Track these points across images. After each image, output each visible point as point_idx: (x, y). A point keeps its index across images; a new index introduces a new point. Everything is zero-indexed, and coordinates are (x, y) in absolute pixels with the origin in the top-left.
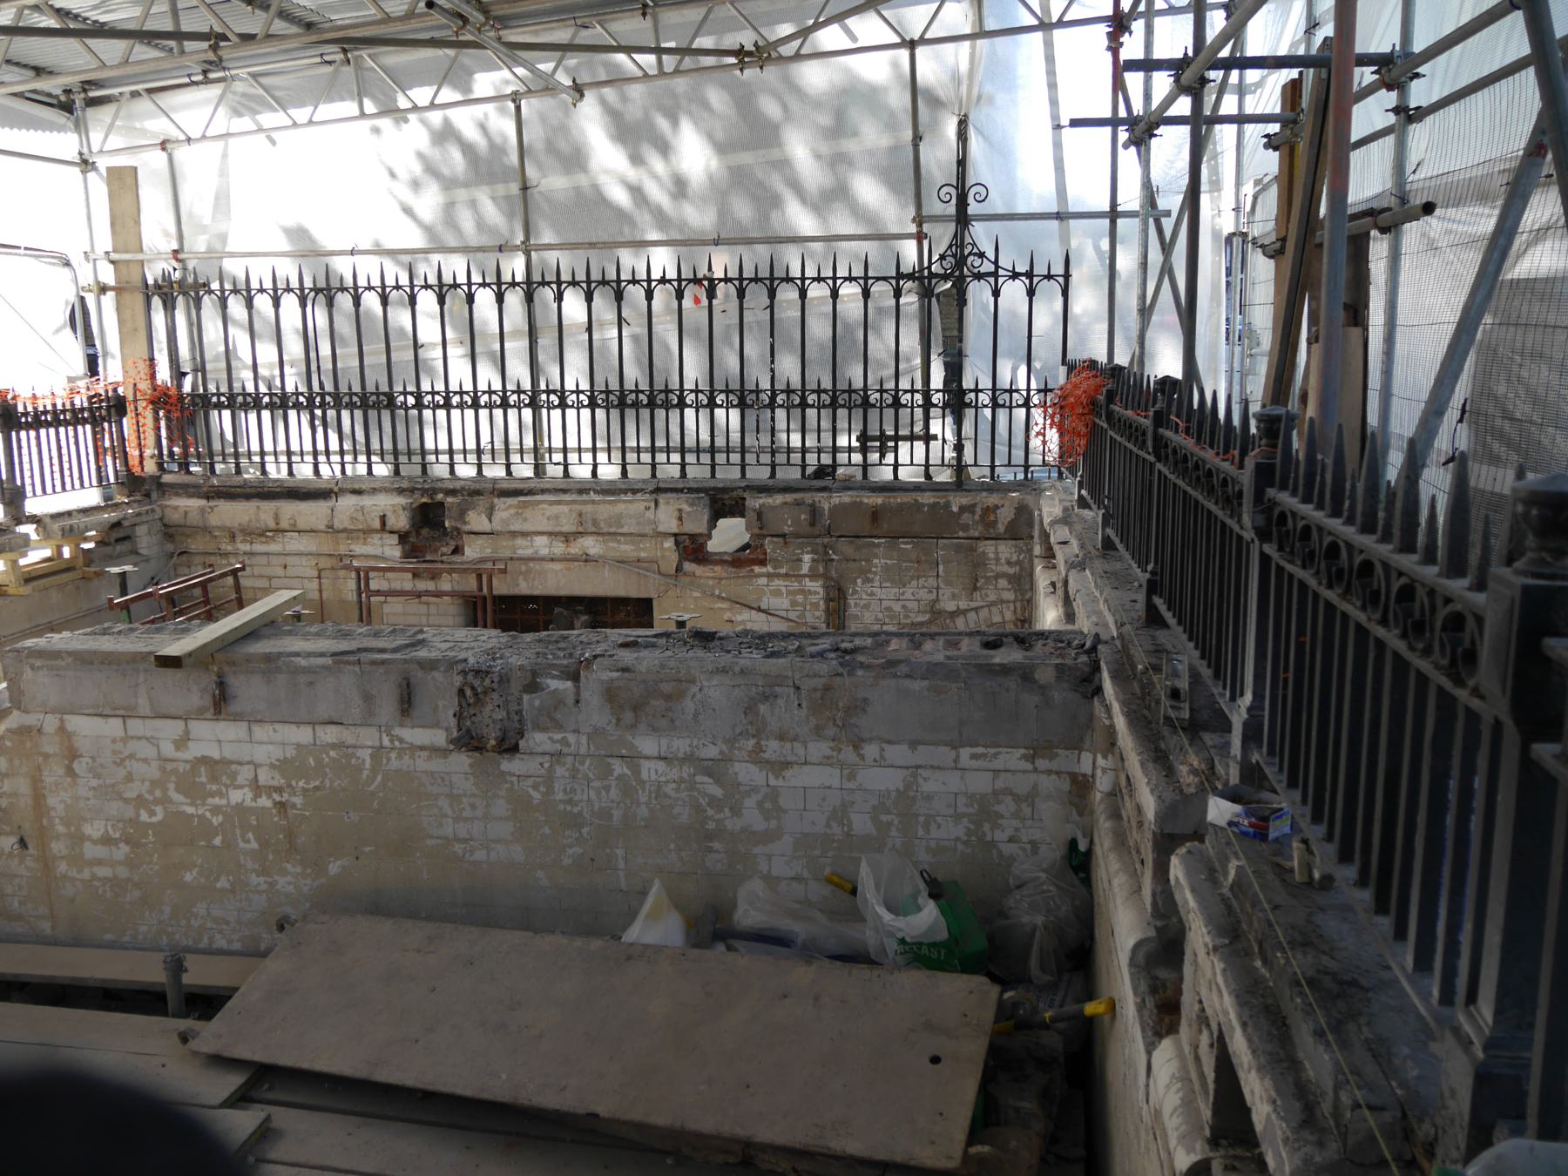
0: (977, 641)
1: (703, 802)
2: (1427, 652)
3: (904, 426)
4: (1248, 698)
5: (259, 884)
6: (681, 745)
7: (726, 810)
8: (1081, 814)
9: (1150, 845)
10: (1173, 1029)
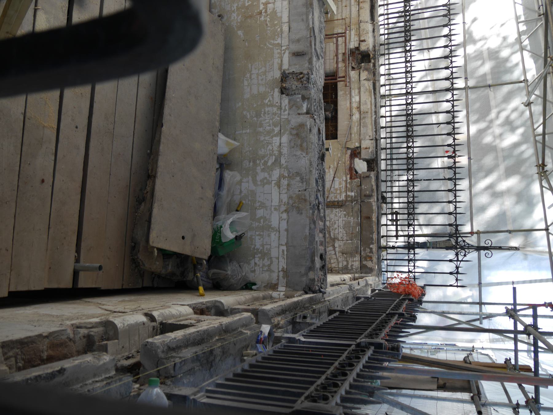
0: (323, 252)
1: (266, 159)
2: (316, 390)
3: (401, 228)
4: (303, 339)
5: (234, 7)
6: (285, 151)
7: (263, 167)
8: (264, 287)
9: (255, 308)
10: (195, 313)
